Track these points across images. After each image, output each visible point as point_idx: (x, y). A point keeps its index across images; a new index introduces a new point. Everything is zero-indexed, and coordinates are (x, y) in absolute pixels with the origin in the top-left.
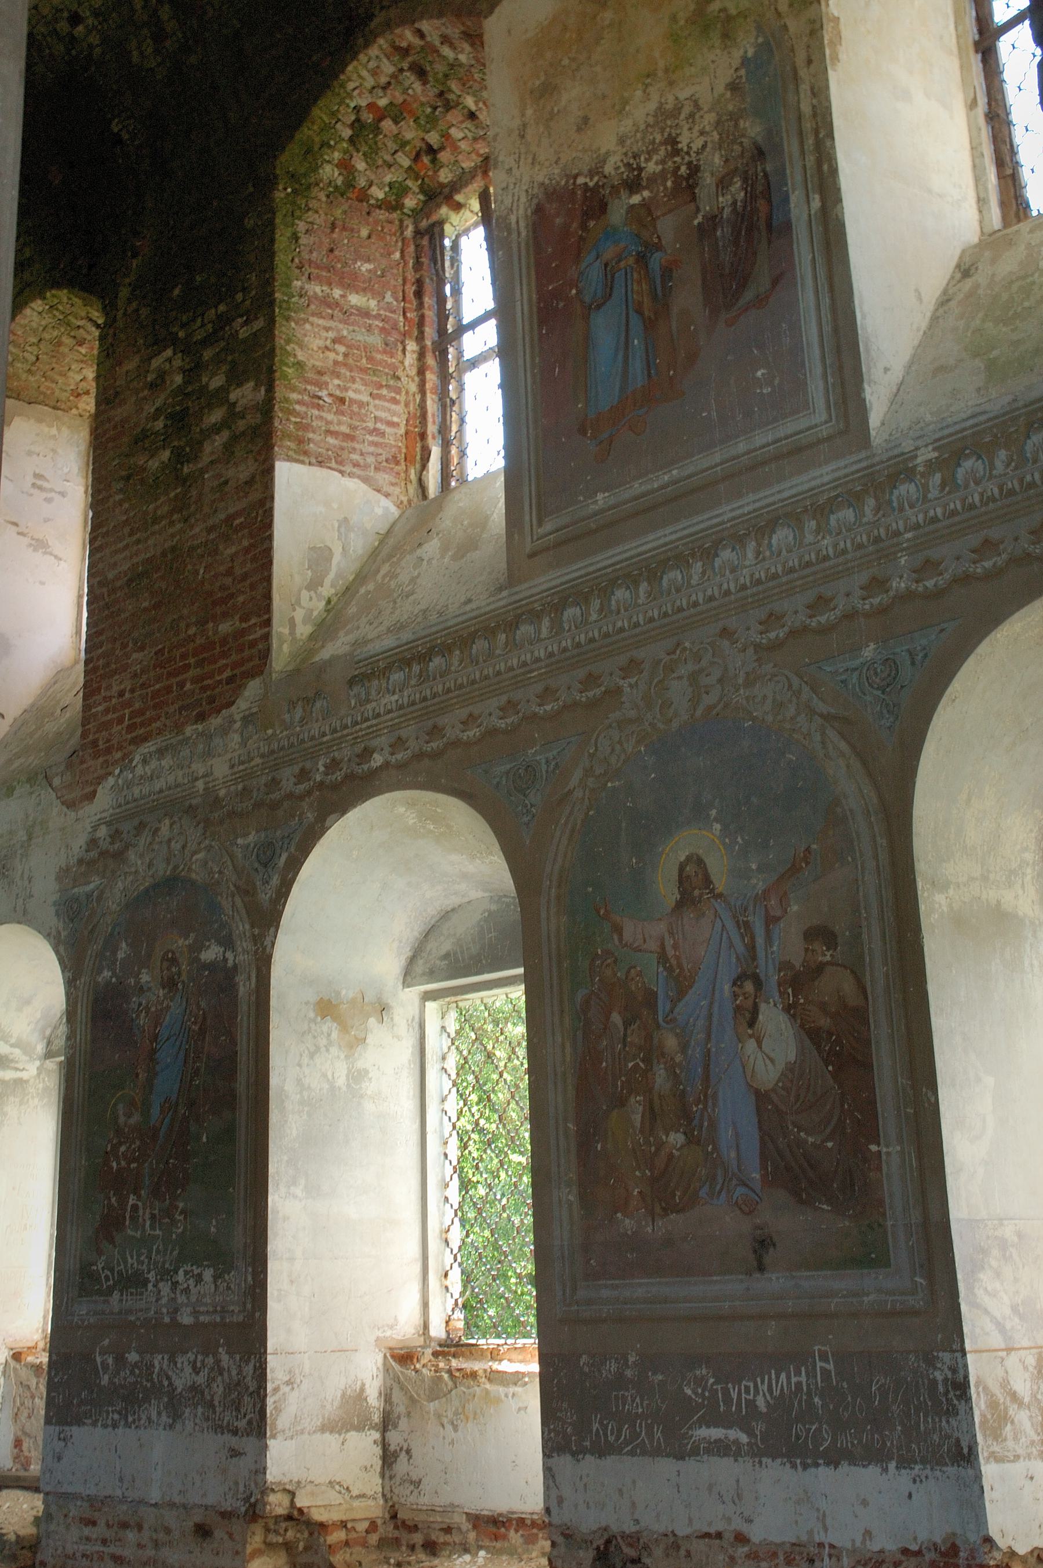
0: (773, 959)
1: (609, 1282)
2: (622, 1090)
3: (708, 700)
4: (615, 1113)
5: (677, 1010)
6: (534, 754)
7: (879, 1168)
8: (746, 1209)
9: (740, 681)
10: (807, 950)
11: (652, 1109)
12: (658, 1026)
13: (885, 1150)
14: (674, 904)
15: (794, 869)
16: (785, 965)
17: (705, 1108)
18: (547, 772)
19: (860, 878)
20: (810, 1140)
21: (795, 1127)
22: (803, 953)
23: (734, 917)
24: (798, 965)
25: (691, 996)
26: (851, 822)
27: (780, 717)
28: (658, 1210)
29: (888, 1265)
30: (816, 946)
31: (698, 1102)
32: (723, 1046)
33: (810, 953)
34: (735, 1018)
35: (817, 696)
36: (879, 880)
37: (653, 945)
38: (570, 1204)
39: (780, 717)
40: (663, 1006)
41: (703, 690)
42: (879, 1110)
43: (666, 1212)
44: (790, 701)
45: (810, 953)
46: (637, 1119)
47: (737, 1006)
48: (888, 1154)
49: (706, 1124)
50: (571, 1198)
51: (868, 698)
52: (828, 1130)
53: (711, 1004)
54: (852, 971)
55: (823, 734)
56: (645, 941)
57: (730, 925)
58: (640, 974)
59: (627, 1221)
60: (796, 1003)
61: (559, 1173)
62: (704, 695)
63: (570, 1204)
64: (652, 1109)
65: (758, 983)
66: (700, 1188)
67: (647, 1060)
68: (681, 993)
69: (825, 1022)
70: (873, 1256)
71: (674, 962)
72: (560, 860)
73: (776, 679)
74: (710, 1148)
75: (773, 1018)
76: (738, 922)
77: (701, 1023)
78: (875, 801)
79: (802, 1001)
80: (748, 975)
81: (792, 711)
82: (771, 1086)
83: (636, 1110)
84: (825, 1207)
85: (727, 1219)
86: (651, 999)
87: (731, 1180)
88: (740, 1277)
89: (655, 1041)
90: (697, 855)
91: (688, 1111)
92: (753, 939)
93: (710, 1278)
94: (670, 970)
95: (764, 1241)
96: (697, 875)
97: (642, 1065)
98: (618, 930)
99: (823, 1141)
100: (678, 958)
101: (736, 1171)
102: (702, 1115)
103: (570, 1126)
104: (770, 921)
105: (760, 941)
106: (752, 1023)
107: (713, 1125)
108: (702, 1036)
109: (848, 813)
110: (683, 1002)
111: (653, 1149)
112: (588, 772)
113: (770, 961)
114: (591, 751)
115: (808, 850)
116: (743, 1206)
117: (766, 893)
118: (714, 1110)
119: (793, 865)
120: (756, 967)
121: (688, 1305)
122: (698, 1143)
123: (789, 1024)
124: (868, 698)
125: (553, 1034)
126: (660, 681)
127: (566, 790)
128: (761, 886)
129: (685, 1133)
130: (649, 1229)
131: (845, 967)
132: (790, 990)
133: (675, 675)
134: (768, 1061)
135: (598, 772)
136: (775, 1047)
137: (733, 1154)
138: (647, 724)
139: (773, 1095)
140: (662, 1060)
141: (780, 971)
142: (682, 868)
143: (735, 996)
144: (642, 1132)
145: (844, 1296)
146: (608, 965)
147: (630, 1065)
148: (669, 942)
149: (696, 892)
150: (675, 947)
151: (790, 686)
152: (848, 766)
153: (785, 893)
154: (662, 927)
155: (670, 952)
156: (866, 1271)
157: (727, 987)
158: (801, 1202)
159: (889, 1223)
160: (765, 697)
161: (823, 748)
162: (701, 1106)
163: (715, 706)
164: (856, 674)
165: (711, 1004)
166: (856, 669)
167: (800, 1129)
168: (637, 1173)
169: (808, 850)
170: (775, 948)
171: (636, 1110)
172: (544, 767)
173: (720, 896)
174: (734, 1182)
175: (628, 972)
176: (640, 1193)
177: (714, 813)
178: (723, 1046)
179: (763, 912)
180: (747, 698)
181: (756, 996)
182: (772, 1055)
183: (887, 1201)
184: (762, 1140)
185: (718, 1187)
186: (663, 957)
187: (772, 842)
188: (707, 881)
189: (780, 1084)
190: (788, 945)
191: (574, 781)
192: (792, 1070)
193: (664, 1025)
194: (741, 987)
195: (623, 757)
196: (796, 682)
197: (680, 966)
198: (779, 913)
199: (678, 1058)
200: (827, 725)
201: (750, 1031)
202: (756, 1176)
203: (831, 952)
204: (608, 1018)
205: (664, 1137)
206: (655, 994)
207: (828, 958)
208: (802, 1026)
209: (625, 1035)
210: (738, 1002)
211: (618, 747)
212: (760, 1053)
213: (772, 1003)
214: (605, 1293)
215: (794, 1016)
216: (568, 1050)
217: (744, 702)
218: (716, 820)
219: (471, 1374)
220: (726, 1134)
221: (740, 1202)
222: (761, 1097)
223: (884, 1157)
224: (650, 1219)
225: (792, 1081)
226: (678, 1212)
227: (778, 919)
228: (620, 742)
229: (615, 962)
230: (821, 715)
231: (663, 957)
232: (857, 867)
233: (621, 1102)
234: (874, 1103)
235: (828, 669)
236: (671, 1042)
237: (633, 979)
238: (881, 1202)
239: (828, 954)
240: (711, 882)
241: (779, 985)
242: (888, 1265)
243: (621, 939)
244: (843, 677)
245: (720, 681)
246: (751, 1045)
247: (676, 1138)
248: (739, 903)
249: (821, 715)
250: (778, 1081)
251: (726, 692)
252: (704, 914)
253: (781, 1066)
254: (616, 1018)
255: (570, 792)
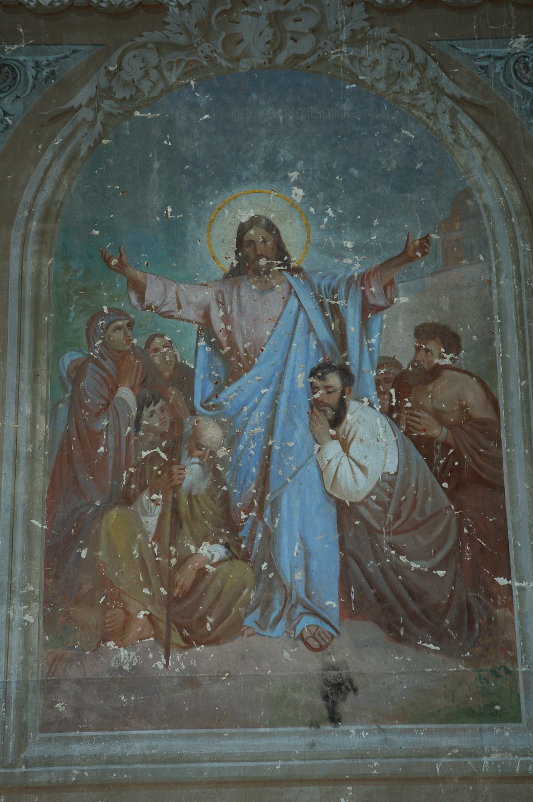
0: (371, 353)
1: (85, 734)
2: (129, 483)
3: (291, 48)
4: (114, 513)
5: (223, 396)
6: (15, 52)
7: (510, 605)
8: (315, 644)
9: (344, 37)
10: (418, 349)
11: (176, 512)
12: (193, 412)
13: (517, 584)
14: (228, 268)
15: (405, 257)
16: (385, 362)
17: (260, 516)
18: (35, 78)
19: (494, 280)
20: (414, 565)
21: (393, 549)
22: (413, 352)
23: (317, 297)
24: (405, 364)
25: (248, 381)
26: (485, 220)
27: (395, 88)
28: (176, 638)
29: (517, 718)
30: (432, 346)
31: (248, 509)
32: (291, 444)
33: (422, 352)
34: (311, 414)
35: (448, 74)
36: (520, 286)
37: (192, 313)
38: (26, 628)
39: (395, 88)
40: (202, 387)
41: (289, 35)
42: (511, 538)
43: (188, 643)
44: (411, 75)
45: (422, 352)
46: (151, 522)
47: (316, 401)
48: (522, 589)
49: (259, 536)
50: (29, 618)
51: (515, 91)
52: (441, 555)
53: (277, 393)
54: (480, 381)
55: (453, 117)
56: (180, 307)
57: (310, 305)
58: (169, 345)
59: (123, 652)
60: (399, 408)
61: (10, 584)
62: (290, 42)
63: (26, 628)
64: (176, 512)
65: (346, 375)
66: (246, 615)
67: (173, 451)
68: (233, 375)
69: (439, 432)
70: (498, 707)
71: (224, 339)
72: (48, 188)
73: (393, 45)
74: (264, 566)
75: (366, 419)
76: (322, 305)
77: (259, 414)
78: (518, 200)
79: (409, 405)
80: (333, 365)
81: (412, 84)
82: (360, 498)
83: (150, 512)
84: (431, 646)
85: (286, 655)
86: (184, 378)
87: (294, 606)
88: (302, 729)
89: (188, 429)
90: (267, 220)
91: (237, 516)
92: (342, 326)
93: (253, 730)
94: (217, 346)
95: (340, 684)
96: (265, 241)
97: (163, 456)
98: (140, 289)
99: (431, 570)
100: (229, 334)
101: (303, 595)
102: (254, 524)
103: (37, 523)
104: (368, 309)
105: (353, 329)
106: (336, 421)
107: (270, 538)
108: (260, 430)
109: (481, 208)
110: (235, 386)
111: (174, 561)
112: (106, 93)
113: (366, 355)
114: (111, 69)
115: (426, 239)
116: (311, 641)
117: (364, 279)
118: (273, 522)
119: (405, 252)
120: (346, 359)
121: (217, 764)
122: (246, 557)
123: (389, 428)
124: (515, 91)
125: (18, 404)
126: (224, 12)
127: (68, 106)
128: (357, 269)
129: (227, 546)
130: (160, 665)
131: (471, 375)
132: (393, 391)
133: (249, 9)
134: (356, 469)
135: (119, 95)
136: (370, 452)
137: (299, 576)
138: (202, 55)
139: (363, 510)
140: (198, 453)
141: (379, 367)
142: (242, 230)
143: (314, 388)
144: (157, 537)
145: (454, 756)
146: (119, 328)
147: (144, 454)
148: (217, 314)
149: (263, 262)
150: (226, 319)
151: (412, 59)
152: (484, 159)
153: (392, 282)
154: (208, 295)
155: (218, 326)
156: (487, 726)
157: (301, 378)
158: (398, 639)
159: (521, 669)
160: (376, 62)
161: (452, 133)
162: (253, 514)
163: (302, 57)
164: (499, 65)
165: (277, 393)
166: (501, 58)
167: (400, 552)
168: (146, 591)
169: (426, 239)
170: (373, 341)
171: (150, 512)
172: (31, 72)
173: (298, 270)
174: (300, 609)
175: (151, 339)
176: (149, 617)
177: (294, 175)
178: (291, 444)
179: (359, 298)
180: (352, 58)
181: (343, 393)
182: (363, 462)
183: (519, 644)
184: (344, 565)
185: (274, 615)
186: (206, 328)
187: (376, 222)
188: (280, 251)
189: (374, 498)
190: (394, 337)
191: (82, 96)
192: (392, 484)
193: (204, 411)
194: (322, 378)
195: (161, 86)
196: (420, 56)
197: (231, 342)
198: (381, 302)
199: (222, 453)
200: (458, 108)
201: (332, 432)
202: (333, 604)
203: (451, 355)
204: (113, 391)
205: (193, 548)
206: (190, 374)
207: (447, 361)
208: (407, 433)
209: (139, 418)
210: (316, 396)
211: (154, 74)
212: (345, 460)
213: (366, 403)
214: (76, 749)
215: (397, 421)
216: (42, 426)
217: (347, 61)
218: (297, 183)
219: (375, 63)
220: (289, 553)
221: (306, 634)
222: (345, 512)
223: (515, 593)
224: (161, 651)
225: (390, 495)
226: (208, 643)
227: (378, 309)
228: (158, 67)
229: (130, 325)
230: (452, 98)
231: (206, 328)
232: (490, 269)
233: (127, 499)
234: (505, 528)
235: (464, 50)
236: (212, 433)
237: (156, 350)
238: (510, 645)
239: (448, 356)
240: (287, 254)
241: (378, 383)
242: (517, 718)
243: (141, 298)
244: (485, 63)
245: (313, 31)
246: (333, 449)
247: (212, 551)
248: (325, 283)
249: (452, 98)
250: (371, 493)
251: (321, 44)
252: (272, 288)
253: (375, 475)
254: (126, 394)
255: (73, 111)
